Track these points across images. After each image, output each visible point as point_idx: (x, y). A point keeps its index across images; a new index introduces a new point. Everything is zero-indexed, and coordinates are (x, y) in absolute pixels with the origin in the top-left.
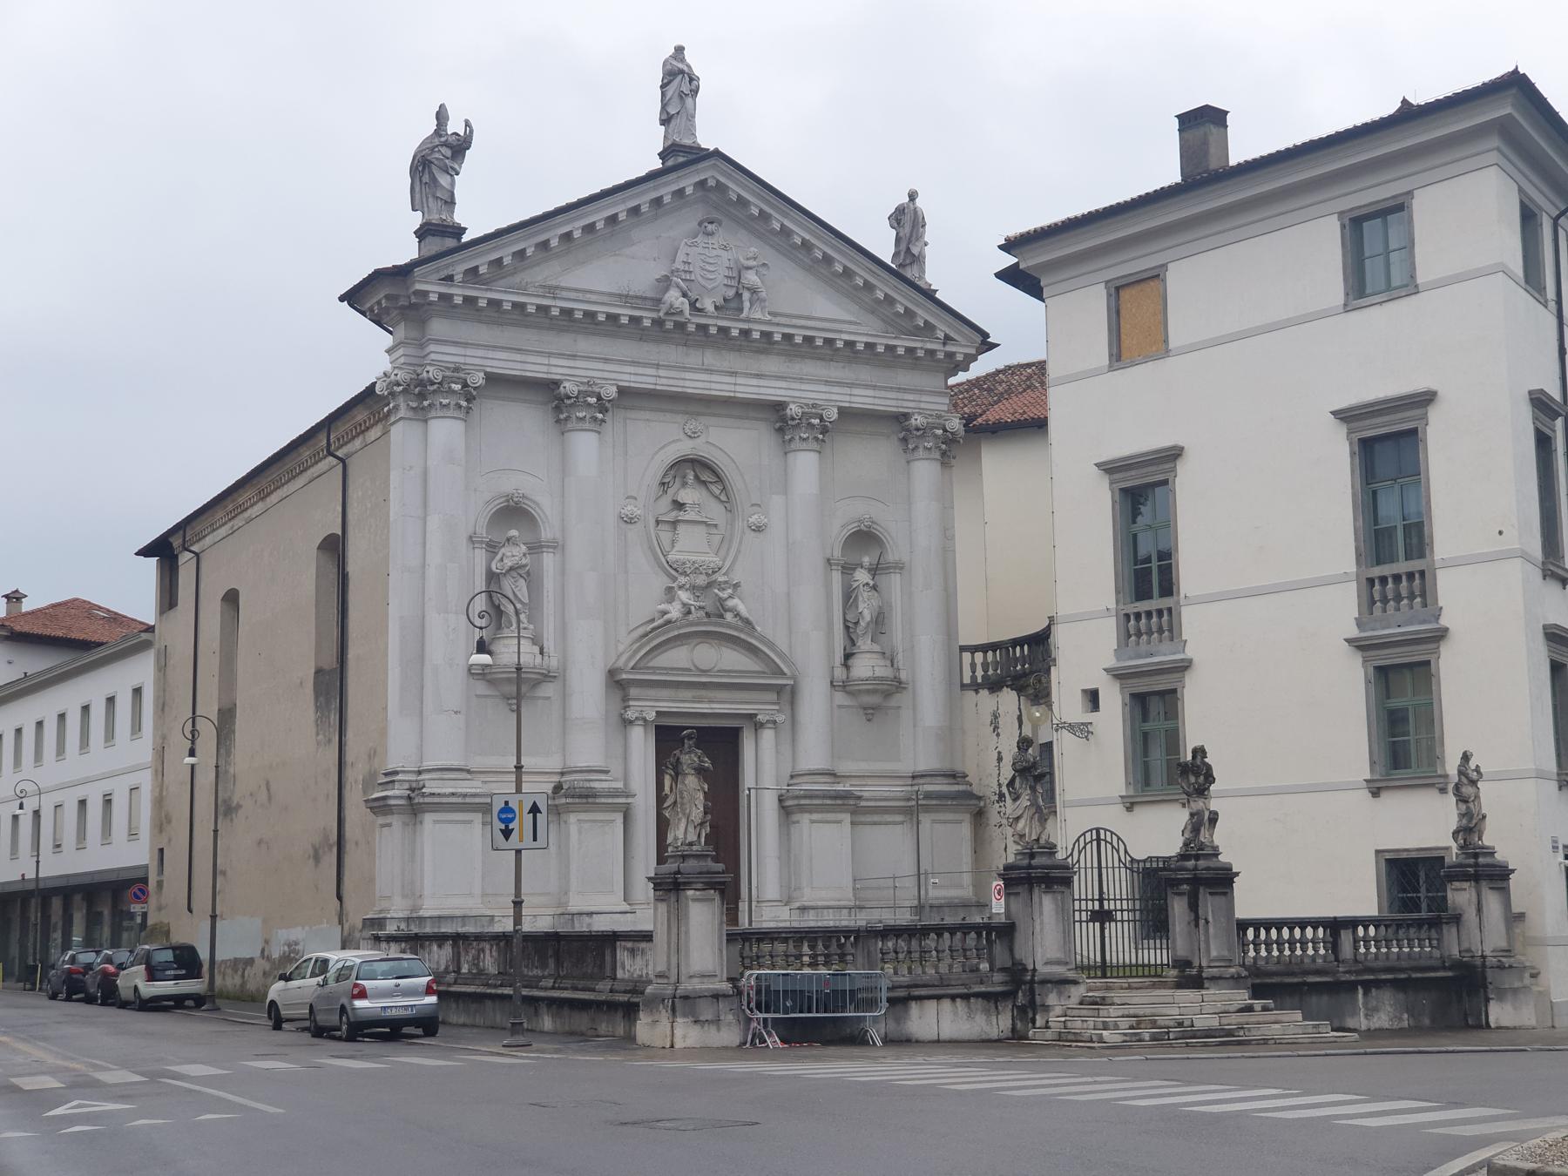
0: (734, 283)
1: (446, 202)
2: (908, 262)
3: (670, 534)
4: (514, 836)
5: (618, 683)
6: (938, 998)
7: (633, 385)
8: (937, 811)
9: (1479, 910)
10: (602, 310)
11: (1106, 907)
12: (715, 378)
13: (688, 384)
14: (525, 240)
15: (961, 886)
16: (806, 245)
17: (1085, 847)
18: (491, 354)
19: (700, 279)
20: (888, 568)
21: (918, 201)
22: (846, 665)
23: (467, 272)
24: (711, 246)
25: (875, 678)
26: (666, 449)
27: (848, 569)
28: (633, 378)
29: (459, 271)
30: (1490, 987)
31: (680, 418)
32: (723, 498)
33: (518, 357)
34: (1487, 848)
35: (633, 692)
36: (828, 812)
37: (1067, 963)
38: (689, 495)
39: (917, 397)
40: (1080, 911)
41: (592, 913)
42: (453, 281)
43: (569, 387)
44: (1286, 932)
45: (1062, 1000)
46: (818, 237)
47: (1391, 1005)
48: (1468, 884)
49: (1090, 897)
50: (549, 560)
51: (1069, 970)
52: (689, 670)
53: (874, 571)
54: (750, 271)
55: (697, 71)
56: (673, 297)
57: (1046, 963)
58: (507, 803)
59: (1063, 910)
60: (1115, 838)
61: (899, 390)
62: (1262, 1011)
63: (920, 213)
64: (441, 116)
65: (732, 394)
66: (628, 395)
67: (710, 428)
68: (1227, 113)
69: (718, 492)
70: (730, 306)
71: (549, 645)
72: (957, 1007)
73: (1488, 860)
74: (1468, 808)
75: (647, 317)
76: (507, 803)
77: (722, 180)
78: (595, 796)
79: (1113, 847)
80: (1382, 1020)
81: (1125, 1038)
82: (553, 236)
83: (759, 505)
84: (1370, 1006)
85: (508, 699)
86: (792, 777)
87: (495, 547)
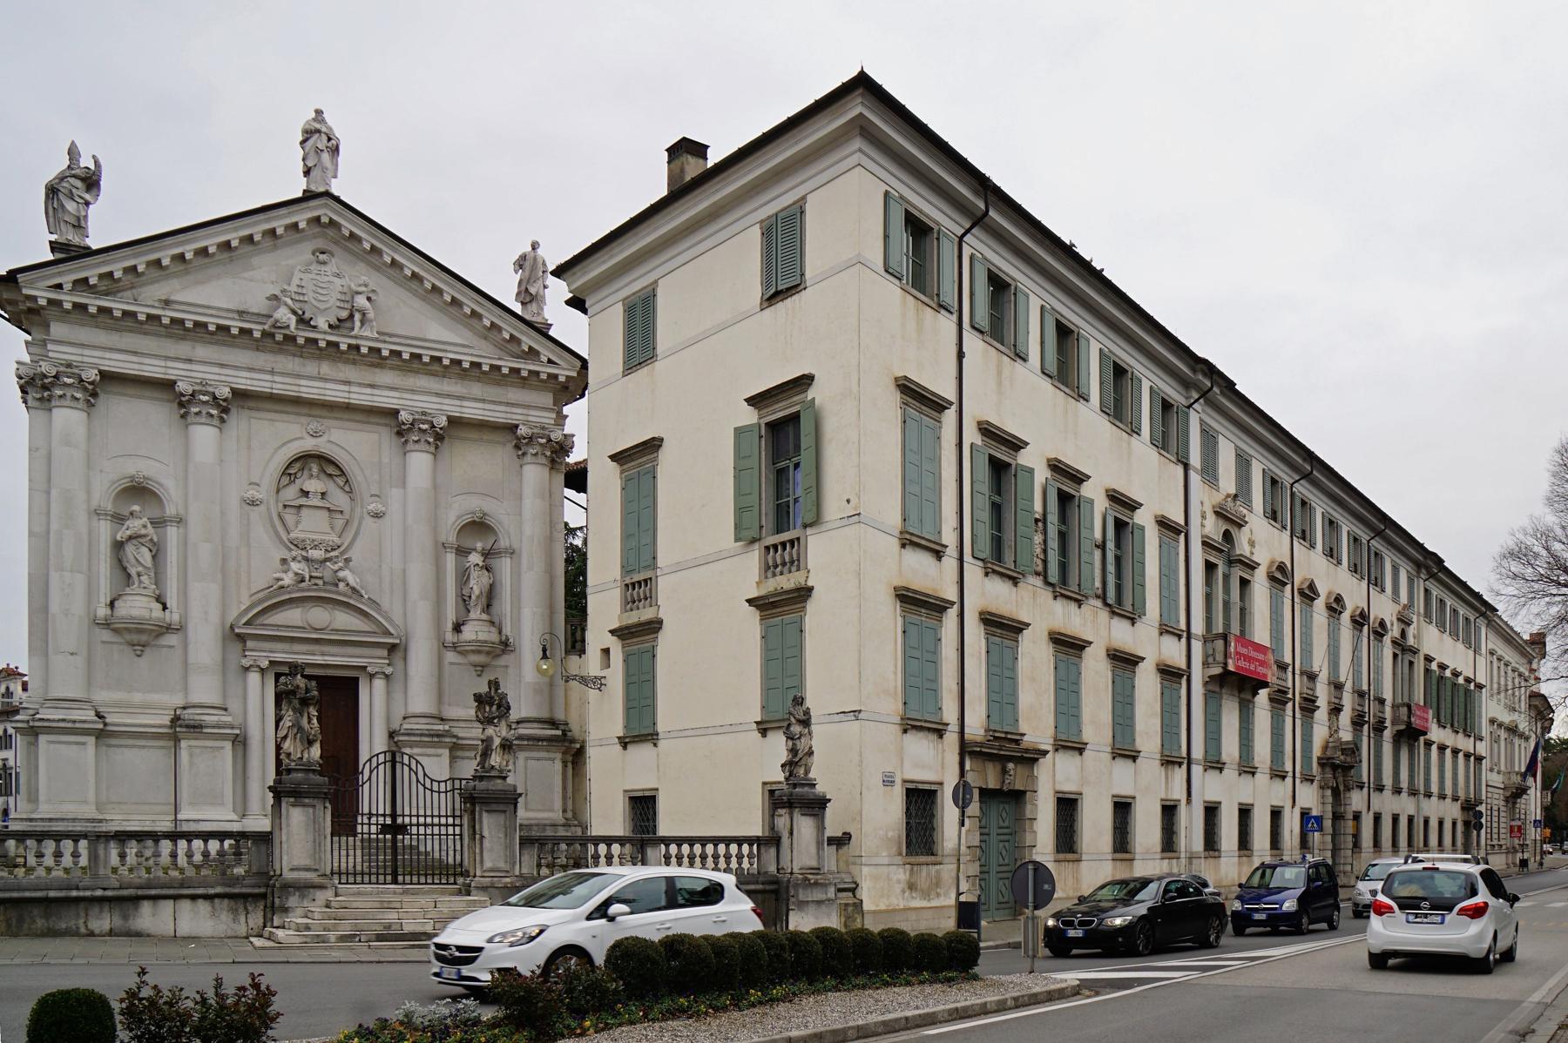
1: (74, 226)
2: (528, 300)
3: (295, 517)
5: (236, 637)
6: (176, 898)
7: (249, 388)
10: (212, 322)
11: (399, 820)
14: (135, 258)
15: (552, 810)
17: (377, 767)
18: (108, 355)
19: (313, 301)
20: (500, 553)
21: (540, 251)
22: (457, 628)
23: (76, 282)
24: (322, 273)
26: (289, 445)
27: (462, 552)
28: (249, 382)
29: (67, 280)
30: (792, 900)
31: (303, 420)
32: (347, 488)
33: (135, 359)
34: (811, 779)
35: (250, 644)
37: (316, 870)
38: (314, 485)
41: (199, 820)
42: (62, 289)
43: (182, 386)
44: (745, 848)
48: (784, 811)
49: (381, 812)
50: (172, 532)
53: (486, 554)
54: (359, 296)
55: (338, 132)
56: (284, 315)
57: (292, 870)
59: (314, 821)
60: (414, 762)
61: (508, 404)
62: (1430, 909)
64: (73, 152)
65: (347, 401)
66: (242, 396)
67: (332, 430)
68: (708, 147)
69: (342, 484)
71: (172, 602)
74: (794, 744)
77: (335, 217)
79: (410, 769)
81: (305, 939)
85: (133, 645)
86: (404, 718)
87: (122, 519)
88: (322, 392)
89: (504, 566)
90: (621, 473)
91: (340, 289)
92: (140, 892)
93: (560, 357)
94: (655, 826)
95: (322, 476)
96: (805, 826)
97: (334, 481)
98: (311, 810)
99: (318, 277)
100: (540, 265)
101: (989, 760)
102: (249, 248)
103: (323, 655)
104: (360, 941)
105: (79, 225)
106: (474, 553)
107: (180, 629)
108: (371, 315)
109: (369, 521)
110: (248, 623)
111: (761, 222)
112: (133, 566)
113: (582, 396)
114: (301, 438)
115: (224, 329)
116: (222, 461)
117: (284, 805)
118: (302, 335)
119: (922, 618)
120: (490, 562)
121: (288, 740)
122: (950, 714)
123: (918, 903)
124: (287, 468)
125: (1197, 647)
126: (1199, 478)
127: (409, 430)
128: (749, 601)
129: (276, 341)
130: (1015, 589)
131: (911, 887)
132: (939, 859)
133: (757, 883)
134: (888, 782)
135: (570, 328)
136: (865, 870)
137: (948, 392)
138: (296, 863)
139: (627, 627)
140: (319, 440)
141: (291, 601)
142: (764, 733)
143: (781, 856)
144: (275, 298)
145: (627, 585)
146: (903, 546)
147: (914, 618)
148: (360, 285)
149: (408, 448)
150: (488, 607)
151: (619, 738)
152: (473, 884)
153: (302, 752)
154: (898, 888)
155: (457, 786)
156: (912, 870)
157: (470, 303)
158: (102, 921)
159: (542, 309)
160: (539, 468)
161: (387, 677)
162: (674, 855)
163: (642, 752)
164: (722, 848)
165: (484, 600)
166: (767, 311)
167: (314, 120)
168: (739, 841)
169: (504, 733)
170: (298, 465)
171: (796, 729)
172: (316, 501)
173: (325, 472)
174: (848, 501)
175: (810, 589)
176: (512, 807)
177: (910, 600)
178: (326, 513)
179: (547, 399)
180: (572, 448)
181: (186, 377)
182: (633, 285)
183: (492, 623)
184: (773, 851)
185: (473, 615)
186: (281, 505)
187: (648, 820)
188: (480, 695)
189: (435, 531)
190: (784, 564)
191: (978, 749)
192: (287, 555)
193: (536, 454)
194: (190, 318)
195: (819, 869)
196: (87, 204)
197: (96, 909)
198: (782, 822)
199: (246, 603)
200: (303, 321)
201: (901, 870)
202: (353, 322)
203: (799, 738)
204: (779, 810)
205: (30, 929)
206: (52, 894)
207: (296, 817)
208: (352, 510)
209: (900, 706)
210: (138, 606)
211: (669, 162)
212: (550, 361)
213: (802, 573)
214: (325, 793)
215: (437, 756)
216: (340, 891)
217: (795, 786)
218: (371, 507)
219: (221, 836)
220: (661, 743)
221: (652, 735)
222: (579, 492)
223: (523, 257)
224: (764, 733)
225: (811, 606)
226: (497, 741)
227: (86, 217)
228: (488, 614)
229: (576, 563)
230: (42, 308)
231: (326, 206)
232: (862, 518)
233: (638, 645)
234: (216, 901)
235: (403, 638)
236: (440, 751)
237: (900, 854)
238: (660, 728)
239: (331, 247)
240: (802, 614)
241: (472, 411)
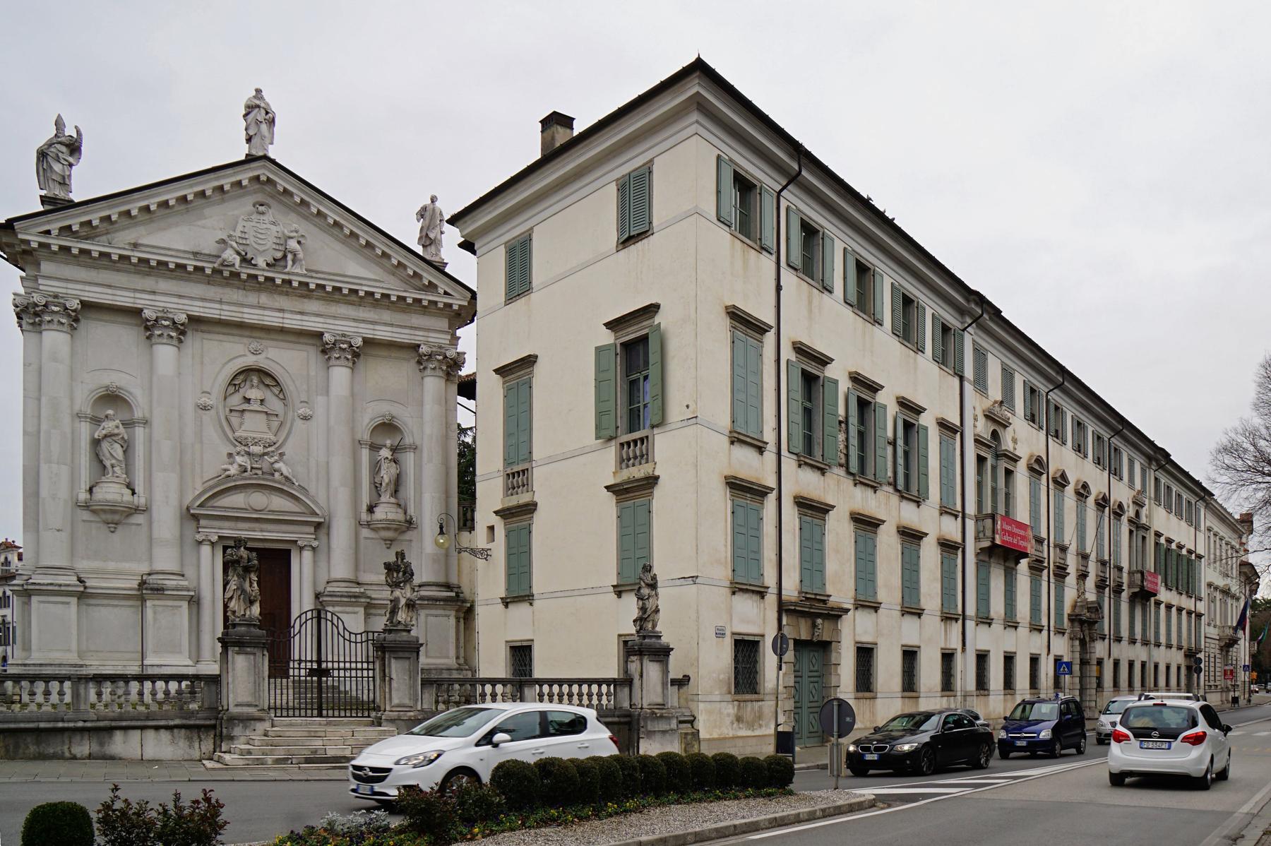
0: (282, 248)
1: (60, 183)
5: (191, 517)
6: (143, 728)
10: (172, 262)
11: (324, 665)
12: (266, 313)
14: (109, 209)
15: (448, 657)
17: (306, 622)
18: (87, 288)
20: (405, 448)
21: (437, 204)
22: (371, 509)
23: (61, 229)
26: (235, 361)
27: (374, 448)
28: (202, 310)
29: (54, 227)
30: (642, 730)
31: (246, 340)
32: (281, 396)
33: (109, 291)
34: (657, 632)
35: (203, 522)
36: (346, 606)
37: (256, 706)
38: (254, 394)
39: (426, 334)
40: (294, 668)
41: (161, 665)
43: (148, 313)
48: (636, 657)
49: (309, 658)
50: (139, 432)
52: (246, 509)
53: (394, 450)
54: (291, 240)
55: (274, 107)
56: (230, 255)
57: (237, 705)
59: (255, 666)
60: (335, 618)
61: (411, 328)
64: (59, 124)
65: (281, 325)
66: (196, 321)
67: (269, 349)
68: (574, 119)
71: (139, 488)
74: (643, 604)
77: (272, 176)
79: (333, 624)
81: (247, 762)
83: (306, 402)
85: (108, 523)
86: (328, 583)
89: (409, 459)
90: (504, 384)
91: (276, 234)
92: (114, 724)
93: (454, 290)
95: (261, 386)
96: (652, 670)
98: (252, 657)
99: (258, 225)
101: (802, 617)
104: (292, 763)
105: (64, 183)
107: (146, 510)
108: (301, 255)
109: (299, 423)
112: (107, 459)
113: (472, 321)
114: (245, 355)
115: (181, 267)
116: (180, 373)
117: (230, 653)
118: (245, 272)
119: (747, 501)
121: (234, 600)
122: (770, 579)
123: (744, 732)
124: (232, 380)
125: (970, 524)
126: (972, 387)
127: (332, 349)
129: (223, 276)
130: (822, 478)
131: (739, 719)
132: (761, 697)
133: (614, 716)
134: (720, 634)
135: (462, 266)
136: (701, 706)
138: (240, 700)
139: (509, 509)
140: (259, 356)
141: (236, 487)
142: (619, 594)
143: (633, 694)
144: (223, 241)
145: (508, 475)
146: (732, 443)
148: (292, 232)
149: (331, 364)
150: (396, 492)
151: (502, 599)
152: (383, 717)
153: (245, 610)
154: (728, 721)
155: (370, 637)
156: (739, 706)
157: (381, 246)
158: (83, 747)
159: (440, 251)
161: (314, 549)
162: (546, 694)
164: (585, 688)
165: (392, 486)
166: (622, 253)
168: (599, 682)
169: (408, 595)
170: (241, 377)
171: (645, 591)
172: (256, 407)
173: (264, 383)
174: (688, 406)
175: (657, 478)
176: (415, 654)
177: (737, 486)
178: (264, 416)
179: (443, 324)
181: (151, 306)
182: (513, 231)
183: (399, 505)
184: (626, 690)
185: (383, 499)
186: (227, 410)
187: (525, 665)
188: (389, 564)
189: (353, 431)
190: (635, 458)
191: (793, 608)
192: (232, 450)
193: (434, 369)
194: (154, 258)
195: (664, 705)
196: (71, 165)
197: (77, 738)
198: (634, 667)
199: (200, 489)
200: (246, 261)
201: (731, 706)
204: (632, 657)
205: (24, 753)
206: (42, 725)
207: (240, 663)
208: (285, 414)
209: (730, 572)
210: (111, 492)
211: (542, 132)
212: (446, 293)
213: (650, 465)
214: (264, 643)
215: (354, 613)
216: (275, 723)
217: (644, 637)
219: (179, 678)
220: (536, 603)
221: (528, 596)
222: (469, 399)
223: (424, 209)
224: (619, 594)
225: (658, 491)
226: (403, 601)
227: (70, 176)
228: (396, 498)
229: (467, 457)
230: (34, 249)
231: (264, 167)
232: (699, 420)
233: (517, 523)
234: (176, 730)
236: (356, 609)
237: (730, 693)
238: (535, 590)
239: (269, 201)
241: (383, 333)
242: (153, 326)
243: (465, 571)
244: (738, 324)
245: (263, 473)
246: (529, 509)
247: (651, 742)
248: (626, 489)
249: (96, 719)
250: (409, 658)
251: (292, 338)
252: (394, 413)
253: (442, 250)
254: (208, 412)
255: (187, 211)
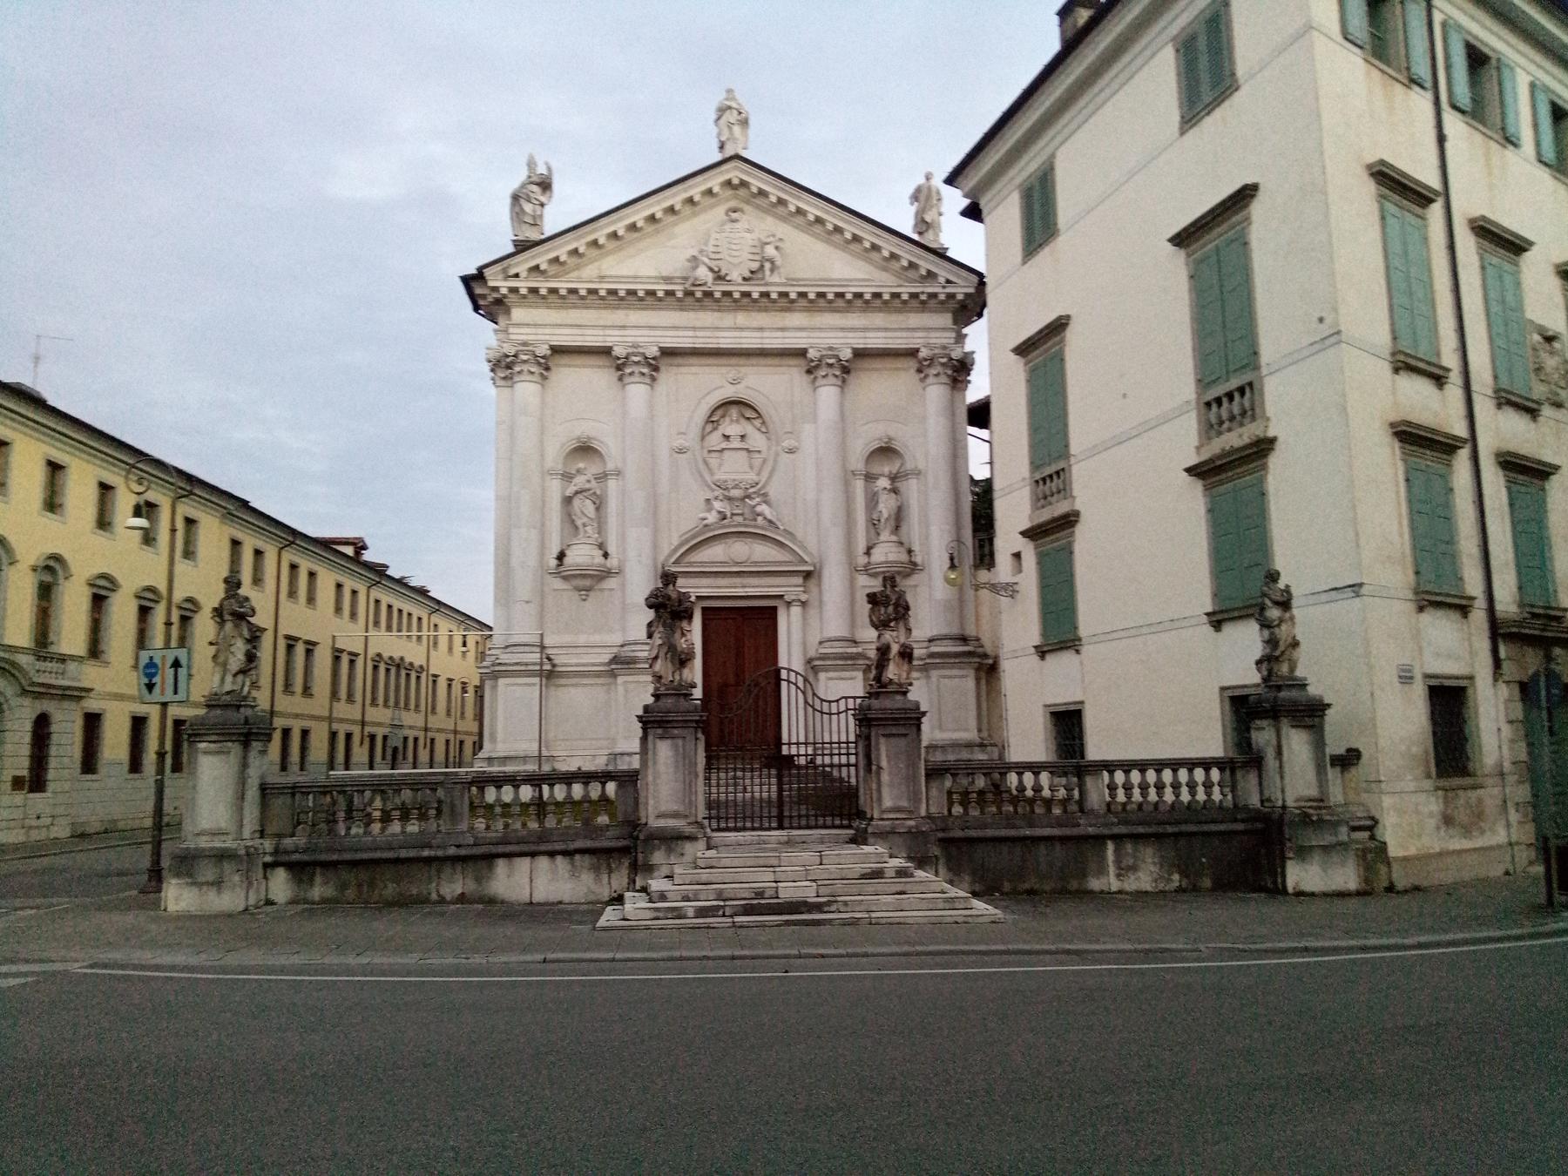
0: (757, 258)
4: (157, 690)
6: (533, 855)
8: (943, 668)
9: (1279, 753)
10: (641, 288)
12: (744, 334)
13: (721, 341)
15: (966, 730)
16: (819, 221)
18: (557, 331)
22: (868, 553)
25: (887, 562)
27: (870, 478)
28: (674, 340)
30: (1288, 844)
31: (724, 370)
32: (764, 430)
34: (1301, 679)
37: (686, 816)
43: (619, 351)
45: (672, 858)
46: (828, 212)
47: (1154, 864)
49: (843, 739)
50: (612, 484)
51: (690, 824)
53: (894, 478)
56: (703, 274)
58: (151, 658)
60: (793, 674)
63: (934, 190)
64: (531, 164)
65: (760, 346)
70: (753, 276)
71: (611, 549)
72: (556, 866)
73: (1294, 694)
74: (1272, 634)
75: (679, 291)
76: (151, 658)
77: (745, 178)
78: (635, 663)
80: (1144, 879)
82: (601, 233)
84: (1123, 865)
85: (580, 591)
88: (738, 340)
89: (911, 487)
90: (1026, 364)
91: (751, 243)
92: (494, 849)
93: (959, 276)
94: (1082, 745)
95: (743, 421)
96: (1297, 744)
97: (753, 424)
98: (680, 742)
99: (731, 235)
100: (934, 194)
101: (1529, 645)
102: (671, 219)
103: (744, 587)
104: (724, 916)
105: (536, 223)
106: (882, 478)
107: (619, 572)
108: (778, 263)
109: (785, 458)
110: (676, 562)
111: (1174, 39)
112: (580, 518)
113: (980, 315)
114: (722, 387)
115: (651, 293)
116: (653, 416)
117: (650, 738)
118: (718, 289)
119: (1428, 460)
120: (898, 484)
121: (659, 661)
122: (1473, 585)
123: (1458, 844)
124: (710, 417)
127: (817, 367)
128: (1189, 470)
129: (694, 297)
130: (1532, 425)
131: (1448, 820)
133: (1236, 820)
134: (1406, 678)
136: (1387, 801)
137: (1432, 180)
138: (663, 808)
139: (1040, 526)
140: (738, 386)
144: (694, 258)
145: (1037, 482)
146: (1396, 370)
147: (1423, 464)
148: (768, 237)
149: (817, 384)
150: (897, 529)
151: (1036, 647)
152: (870, 830)
153: (673, 673)
154: (1432, 823)
156: (1445, 798)
157: (869, 236)
158: (454, 885)
159: (938, 236)
160: (942, 387)
161: (804, 604)
162: (1136, 784)
163: (1062, 662)
164: (1135, 776)
165: (892, 523)
167: (727, 99)
169: (902, 640)
170: (719, 412)
171: (1274, 613)
172: (736, 444)
173: (743, 416)
174: (1321, 320)
175: (1272, 441)
176: (914, 729)
177: (1412, 437)
178: (744, 453)
179: (946, 319)
180: (972, 365)
181: (620, 343)
182: (1027, 167)
183: (901, 543)
184: (1252, 778)
185: (882, 538)
186: (705, 451)
187: (1074, 739)
188: (874, 594)
189: (844, 459)
190: (1232, 418)
191: (1517, 630)
192: (709, 495)
193: (937, 375)
194: (622, 288)
195: (1322, 800)
196: (542, 205)
197: (448, 870)
198: (1263, 736)
199: (676, 542)
201: (1433, 799)
202: (764, 271)
203: (1279, 625)
204: (1258, 722)
205: (381, 895)
206: (404, 854)
207: (664, 751)
208: (769, 448)
209: (1411, 577)
210: (582, 555)
211: (1061, 25)
212: (948, 281)
214: (697, 722)
215: (851, 679)
216: (713, 843)
217: (1279, 688)
218: (786, 444)
220: (1084, 649)
221: (1073, 640)
222: (981, 427)
223: (918, 190)
225: (1274, 461)
226: (895, 648)
227: (541, 216)
229: (984, 494)
230: (505, 296)
231: (736, 168)
232: (1344, 337)
233: (1051, 543)
234: (577, 857)
235: (818, 565)
236: (854, 674)
237: (1428, 776)
238: (1083, 631)
239: (742, 205)
240: (1262, 473)
241: (876, 341)
242: (624, 364)
243: (985, 611)
244: (1387, 192)
245: (745, 519)
246: (1068, 521)
247: (1307, 867)
248: (1221, 466)
249: (472, 842)
250: (229, 752)
251: (776, 361)
252: (892, 434)
253: (941, 234)
254: (684, 455)
255: (657, 231)
